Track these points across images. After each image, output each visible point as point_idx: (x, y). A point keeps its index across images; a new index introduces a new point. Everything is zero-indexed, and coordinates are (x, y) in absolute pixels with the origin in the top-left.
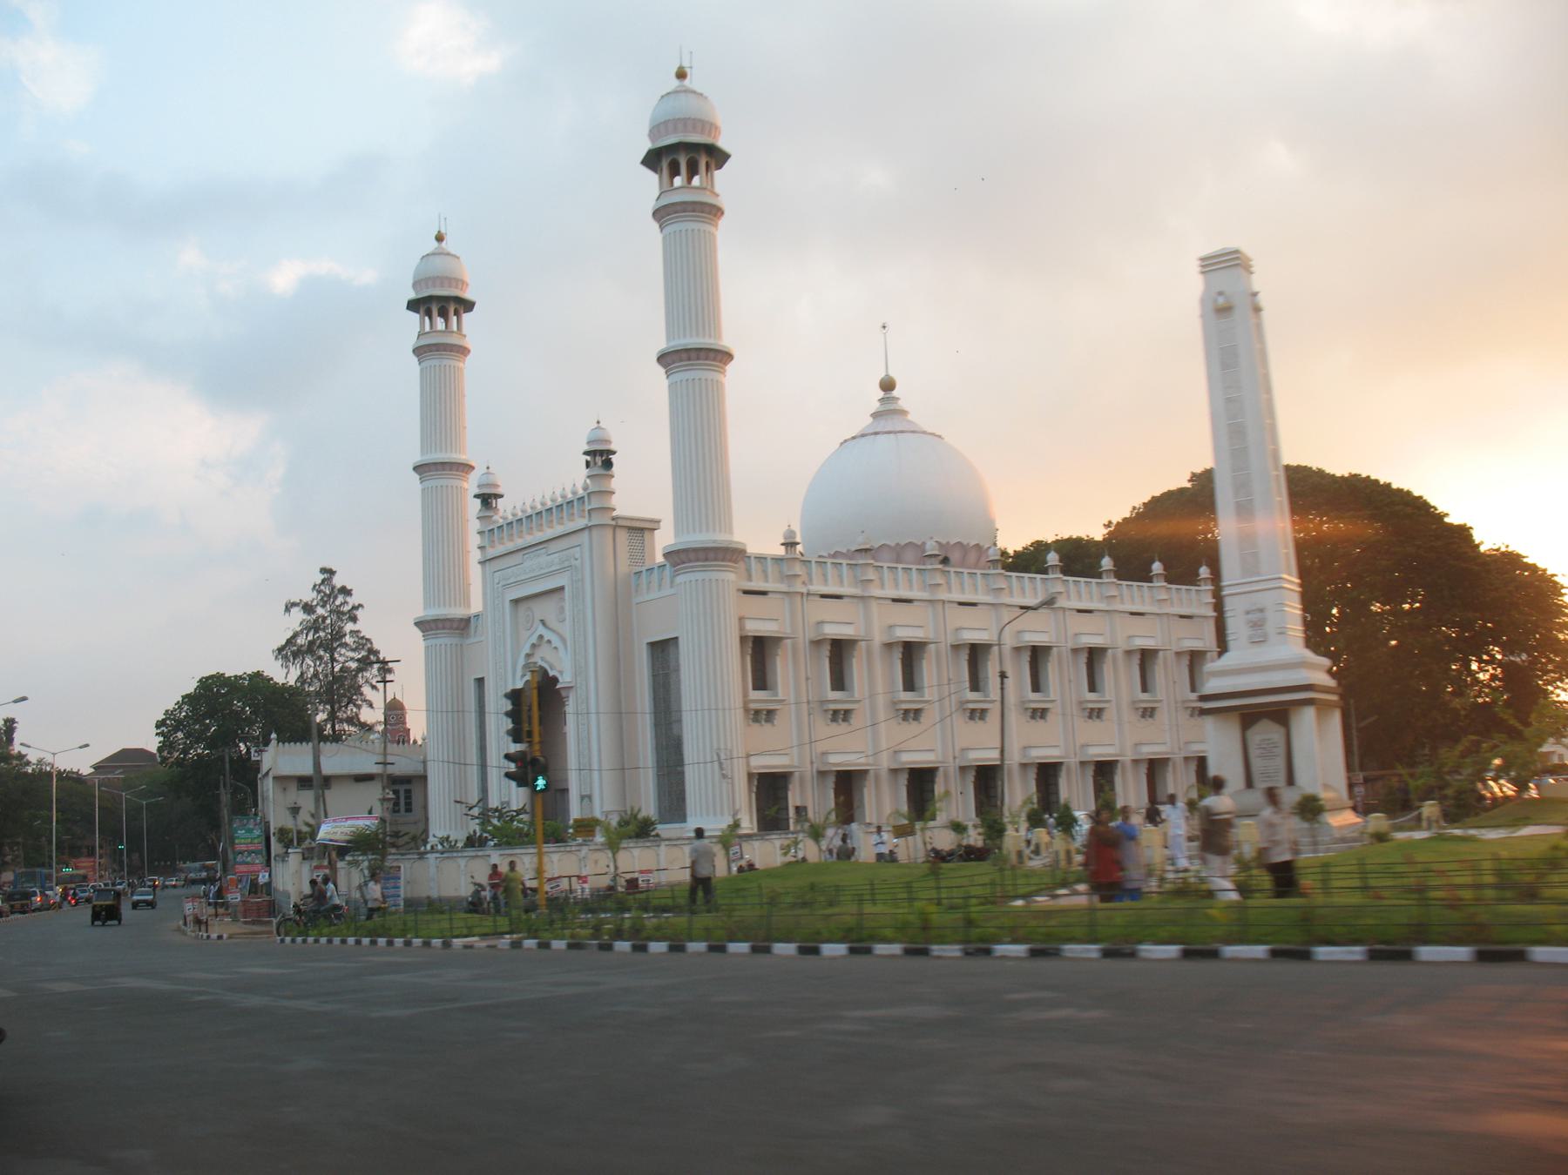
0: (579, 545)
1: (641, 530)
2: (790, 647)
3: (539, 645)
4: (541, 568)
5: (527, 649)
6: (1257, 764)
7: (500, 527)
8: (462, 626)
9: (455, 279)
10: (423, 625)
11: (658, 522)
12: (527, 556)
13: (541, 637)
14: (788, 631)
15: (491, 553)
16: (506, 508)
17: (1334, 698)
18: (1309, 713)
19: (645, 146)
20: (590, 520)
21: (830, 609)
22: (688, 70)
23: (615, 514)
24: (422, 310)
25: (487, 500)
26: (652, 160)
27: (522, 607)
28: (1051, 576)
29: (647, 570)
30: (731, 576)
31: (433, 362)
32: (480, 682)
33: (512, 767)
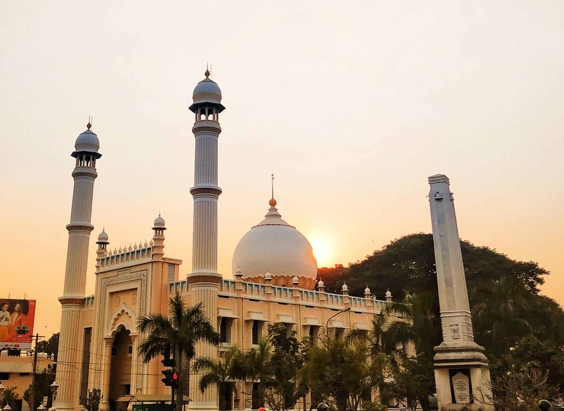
0: (147, 270)
1: (174, 264)
2: (236, 322)
4: (127, 279)
5: (115, 316)
6: (457, 393)
7: (108, 258)
8: (82, 302)
10: (63, 301)
11: (181, 261)
12: (120, 272)
13: (123, 311)
14: (292, 322)
15: (102, 270)
16: (111, 249)
17: (487, 364)
18: (478, 372)
19: (192, 102)
20: (153, 259)
21: (282, 310)
22: (210, 72)
23: (164, 256)
24: (78, 158)
25: (103, 243)
26: (194, 108)
27: (115, 296)
28: (344, 295)
29: (176, 283)
31: (82, 180)
32: (88, 331)
33: (164, 377)
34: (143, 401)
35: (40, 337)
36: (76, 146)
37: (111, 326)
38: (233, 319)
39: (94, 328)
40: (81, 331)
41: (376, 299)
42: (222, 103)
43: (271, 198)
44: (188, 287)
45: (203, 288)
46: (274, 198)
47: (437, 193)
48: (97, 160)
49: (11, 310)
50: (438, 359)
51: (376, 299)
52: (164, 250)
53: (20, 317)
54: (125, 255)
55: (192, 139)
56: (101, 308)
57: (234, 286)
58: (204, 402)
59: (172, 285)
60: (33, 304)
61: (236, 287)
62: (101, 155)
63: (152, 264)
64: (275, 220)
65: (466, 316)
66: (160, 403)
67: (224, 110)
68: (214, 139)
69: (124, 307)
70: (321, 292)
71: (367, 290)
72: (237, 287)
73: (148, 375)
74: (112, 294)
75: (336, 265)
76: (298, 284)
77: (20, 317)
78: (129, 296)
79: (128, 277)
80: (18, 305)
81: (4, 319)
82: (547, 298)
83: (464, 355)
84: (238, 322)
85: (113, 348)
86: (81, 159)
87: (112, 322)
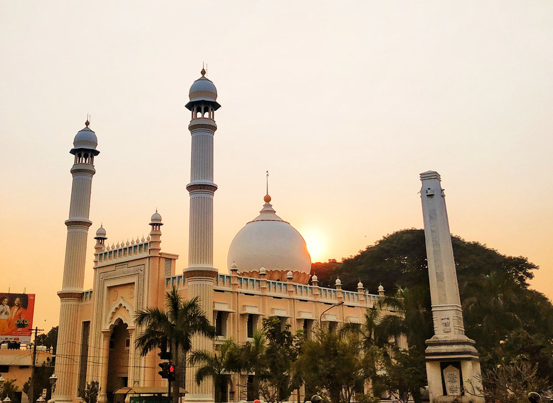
0: (144, 265)
1: (170, 259)
2: (232, 316)
3: (119, 309)
5: (113, 310)
6: (448, 385)
7: (106, 253)
8: (80, 296)
9: (93, 142)
10: (62, 295)
11: (178, 256)
12: (117, 267)
13: (121, 305)
14: (287, 316)
15: (100, 264)
16: (109, 244)
17: (478, 357)
18: (469, 364)
19: (188, 100)
20: (150, 254)
21: (277, 304)
22: (206, 71)
23: (160, 252)
24: (77, 155)
25: (101, 239)
26: (190, 106)
27: (112, 291)
28: (337, 290)
30: (212, 284)
31: (80, 176)
32: (86, 325)
33: (161, 370)
34: (140, 394)
35: (39, 330)
36: (74, 143)
37: (108, 320)
38: (228, 313)
39: (92, 322)
40: (80, 324)
41: (369, 293)
42: (218, 101)
43: (266, 194)
44: (184, 281)
45: (199, 283)
46: (269, 194)
47: (429, 189)
48: (95, 157)
49: (11, 304)
50: (430, 352)
51: (369, 293)
52: (161, 245)
53: (20, 311)
54: (123, 250)
55: (188, 136)
56: (99, 302)
57: (229, 281)
58: (200, 394)
59: (168, 279)
60: (32, 298)
61: (231, 281)
62: (99, 152)
63: (149, 259)
64: (269, 216)
65: (457, 310)
66: (156, 395)
67: (220, 108)
68: (209, 136)
69: (121, 301)
70: (315, 286)
71: (360, 285)
72: (233, 281)
73: (145, 367)
74: (110, 288)
75: (330, 260)
76: (292, 278)
77: (20, 311)
78: (127, 290)
79: (126, 272)
80: (18, 299)
81: (4, 313)
82: (536, 292)
83: (455, 348)
84: (234, 315)
85: (110, 341)
86: (80, 156)
87: (110, 315)
